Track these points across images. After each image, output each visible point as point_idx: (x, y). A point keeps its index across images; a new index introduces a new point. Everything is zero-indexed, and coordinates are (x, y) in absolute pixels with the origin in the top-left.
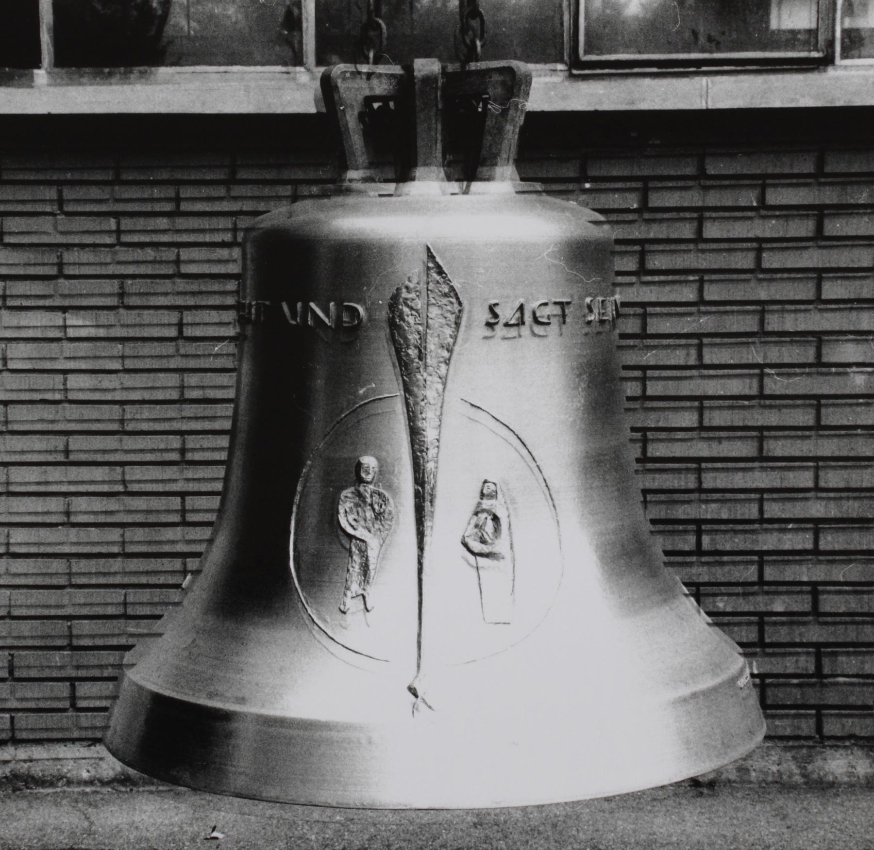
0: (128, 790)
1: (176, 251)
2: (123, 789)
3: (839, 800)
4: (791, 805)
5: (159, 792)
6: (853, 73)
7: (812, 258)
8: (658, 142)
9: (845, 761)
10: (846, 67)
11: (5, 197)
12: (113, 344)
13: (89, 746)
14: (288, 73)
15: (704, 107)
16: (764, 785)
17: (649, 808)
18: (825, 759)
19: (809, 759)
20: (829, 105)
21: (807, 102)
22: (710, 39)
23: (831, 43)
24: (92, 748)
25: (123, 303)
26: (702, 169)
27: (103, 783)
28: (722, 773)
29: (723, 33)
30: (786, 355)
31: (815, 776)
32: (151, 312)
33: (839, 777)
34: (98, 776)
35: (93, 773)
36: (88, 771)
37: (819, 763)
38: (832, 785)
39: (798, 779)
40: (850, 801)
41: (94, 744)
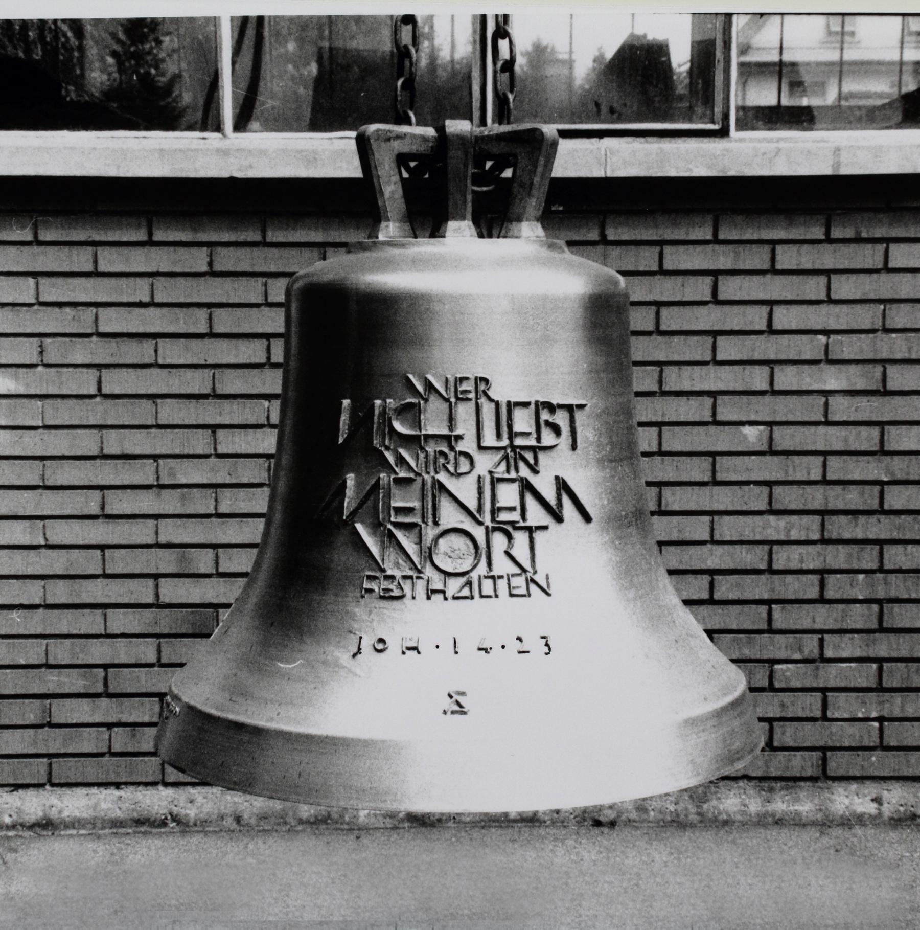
0: (50, 833)
6: (743, 145)
8: (561, 208)
9: (739, 800)
10: (741, 140)
13: (12, 791)
14: (204, 138)
15: (603, 176)
20: (721, 175)
21: (782, 168)
22: (612, 110)
23: (726, 117)
24: (15, 793)
25: (42, 361)
26: (603, 235)
28: (622, 813)
30: (682, 410)
34: (21, 821)
36: (10, 816)
37: (714, 802)
39: (693, 818)
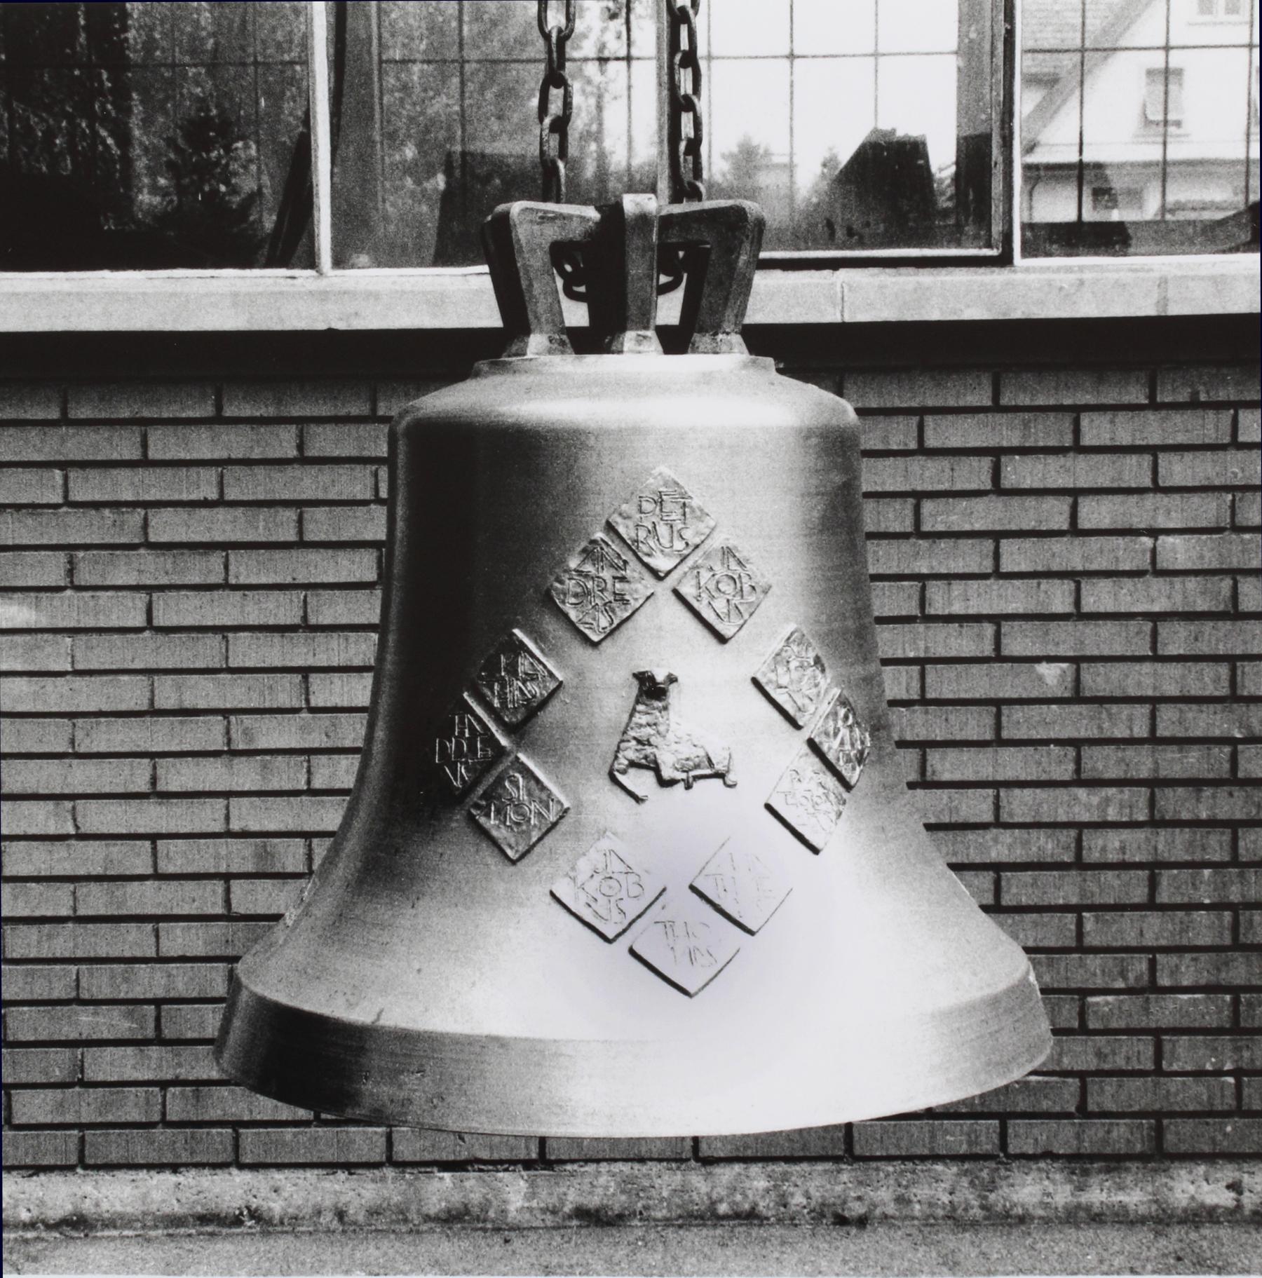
1: (143, 512)
2: (75, 1234)
3: (1029, 1241)
4: (964, 1245)
5: (122, 1238)
7: (985, 515)
11: (10, 414)
12: (59, 637)
13: (30, 1176)
16: (932, 1221)
17: (776, 1254)
18: (1013, 1186)
19: (992, 1186)
20: (1001, 317)
22: (850, 232)
24: (35, 1178)
25: (72, 582)
27: (49, 1227)
29: (868, 224)
31: (999, 1208)
32: (110, 593)
33: (1031, 1209)
35: (35, 1212)
36: (29, 1210)
37: (1005, 1190)
38: (1023, 1220)
39: (977, 1212)
40: (1044, 1241)
41: (36, 1174)
